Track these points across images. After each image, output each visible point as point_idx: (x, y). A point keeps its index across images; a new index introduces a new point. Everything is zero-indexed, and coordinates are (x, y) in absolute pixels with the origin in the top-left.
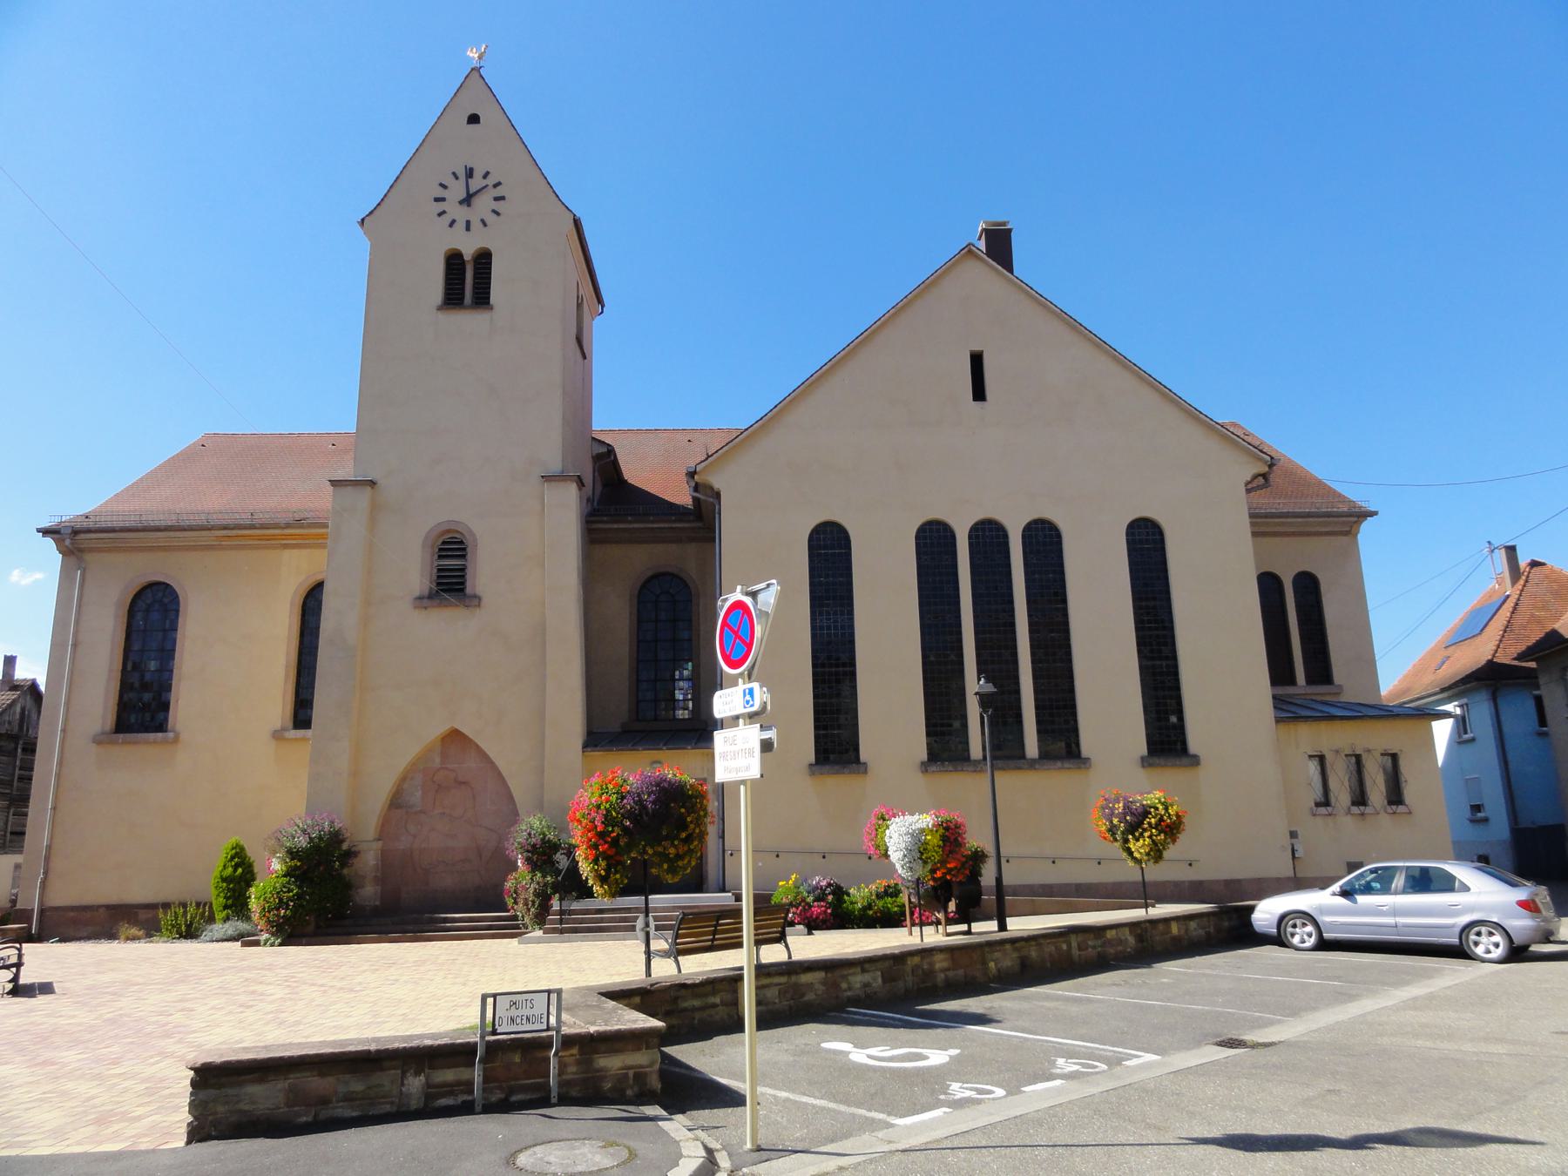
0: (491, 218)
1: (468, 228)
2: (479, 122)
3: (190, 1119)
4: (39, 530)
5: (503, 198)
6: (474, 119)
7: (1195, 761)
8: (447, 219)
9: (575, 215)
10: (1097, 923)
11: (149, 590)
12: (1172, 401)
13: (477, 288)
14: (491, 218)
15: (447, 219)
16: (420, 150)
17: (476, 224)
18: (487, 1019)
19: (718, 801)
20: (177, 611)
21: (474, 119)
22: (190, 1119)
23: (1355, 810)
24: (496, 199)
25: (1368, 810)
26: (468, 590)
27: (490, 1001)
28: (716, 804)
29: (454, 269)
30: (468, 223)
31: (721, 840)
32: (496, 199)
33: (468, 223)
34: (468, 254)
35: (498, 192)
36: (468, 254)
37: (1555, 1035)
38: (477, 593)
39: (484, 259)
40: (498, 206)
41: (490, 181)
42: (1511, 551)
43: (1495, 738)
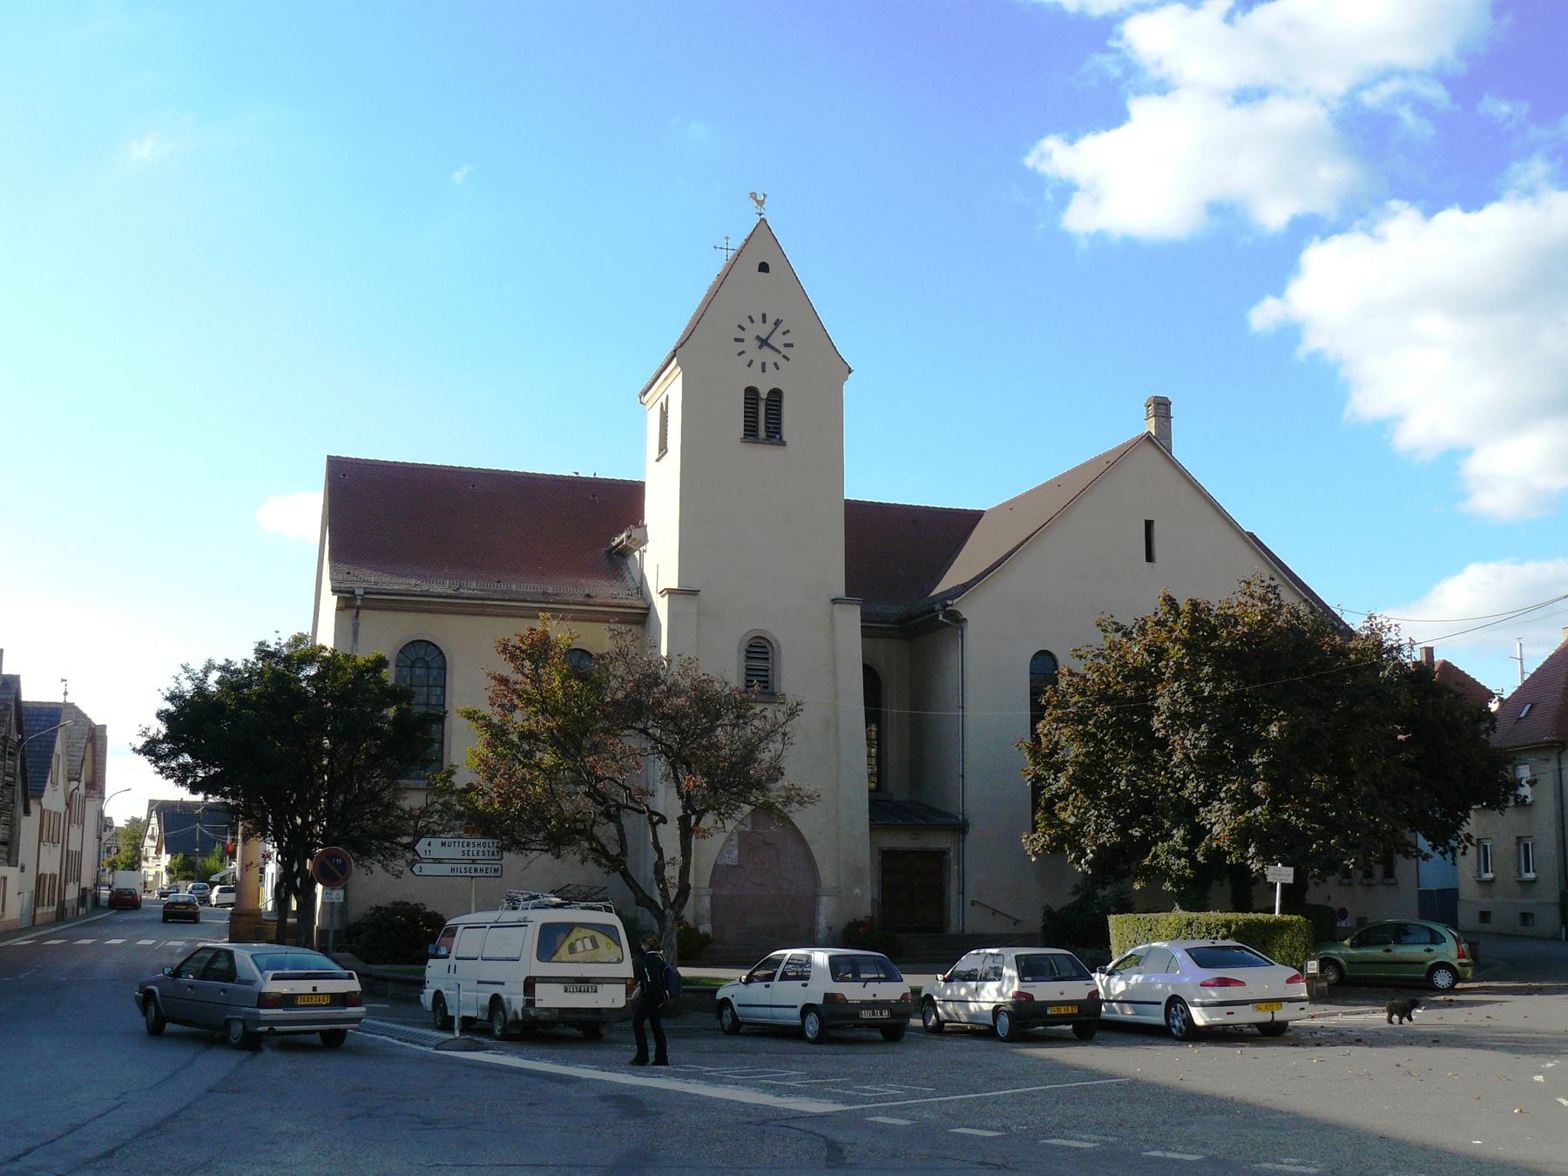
0: (746, 324)
1: (737, 340)
2: (768, 272)
3: (428, 910)
5: (764, 316)
7: (783, 444)
8: (745, 359)
10: (1128, 1045)
12: (1176, 467)
15: (745, 359)
18: (652, 1035)
21: (764, 267)
23: (1365, 881)
25: (1373, 882)
28: (956, 867)
29: (775, 428)
30: (741, 340)
33: (741, 340)
36: (764, 394)
39: (776, 396)
42: (835, 601)
43: (1556, 814)
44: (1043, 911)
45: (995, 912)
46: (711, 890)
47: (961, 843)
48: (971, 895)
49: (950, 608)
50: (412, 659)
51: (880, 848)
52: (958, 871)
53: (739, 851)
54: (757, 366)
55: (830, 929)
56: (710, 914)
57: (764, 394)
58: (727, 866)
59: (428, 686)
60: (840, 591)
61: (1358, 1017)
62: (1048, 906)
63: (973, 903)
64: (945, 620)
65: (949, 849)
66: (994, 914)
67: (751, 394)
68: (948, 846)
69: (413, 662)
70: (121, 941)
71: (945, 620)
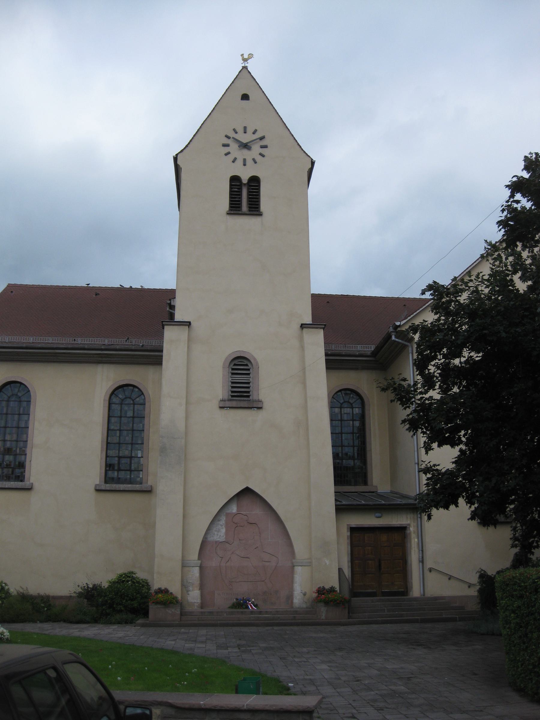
0: (259, 158)
3: (105, 585)
4: (523, 289)
6: (245, 97)
8: (231, 157)
9: (312, 159)
11: (8, 386)
13: (250, 201)
14: (259, 158)
15: (231, 157)
16: (212, 114)
17: (249, 162)
19: (418, 538)
20: (29, 402)
21: (245, 97)
22: (105, 585)
24: (262, 147)
26: (253, 396)
27: (188, 324)
28: (416, 540)
31: (421, 564)
32: (262, 147)
33: (245, 160)
34: (245, 179)
35: (263, 143)
36: (245, 180)
37: (403, 428)
38: (260, 398)
39: (255, 181)
40: (263, 151)
41: (258, 135)
42: (303, 326)
44: (478, 574)
45: (450, 578)
46: (200, 562)
47: (419, 519)
48: (429, 564)
49: (399, 329)
50: (9, 395)
51: (348, 525)
52: (418, 544)
53: (226, 530)
54: (240, 162)
55: (305, 594)
56: (199, 582)
57: (245, 180)
58: (216, 542)
59: (19, 414)
60: (308, 319)
61: (240, 361)
62: (482, 570)
63: (430, 570)
64: (397, 340)
65: (409, 525)
66: (449, 579)
67: (235, 180)
68: (409, 522)
69: (9, 397)
70: (256, 608)
71: (397, 340)
